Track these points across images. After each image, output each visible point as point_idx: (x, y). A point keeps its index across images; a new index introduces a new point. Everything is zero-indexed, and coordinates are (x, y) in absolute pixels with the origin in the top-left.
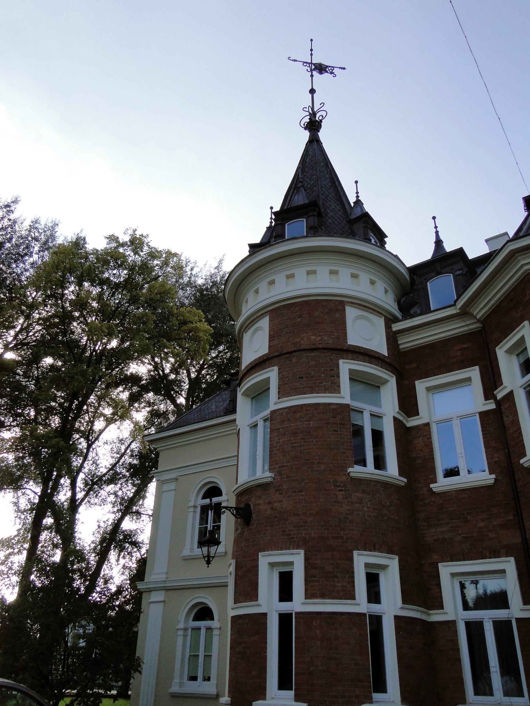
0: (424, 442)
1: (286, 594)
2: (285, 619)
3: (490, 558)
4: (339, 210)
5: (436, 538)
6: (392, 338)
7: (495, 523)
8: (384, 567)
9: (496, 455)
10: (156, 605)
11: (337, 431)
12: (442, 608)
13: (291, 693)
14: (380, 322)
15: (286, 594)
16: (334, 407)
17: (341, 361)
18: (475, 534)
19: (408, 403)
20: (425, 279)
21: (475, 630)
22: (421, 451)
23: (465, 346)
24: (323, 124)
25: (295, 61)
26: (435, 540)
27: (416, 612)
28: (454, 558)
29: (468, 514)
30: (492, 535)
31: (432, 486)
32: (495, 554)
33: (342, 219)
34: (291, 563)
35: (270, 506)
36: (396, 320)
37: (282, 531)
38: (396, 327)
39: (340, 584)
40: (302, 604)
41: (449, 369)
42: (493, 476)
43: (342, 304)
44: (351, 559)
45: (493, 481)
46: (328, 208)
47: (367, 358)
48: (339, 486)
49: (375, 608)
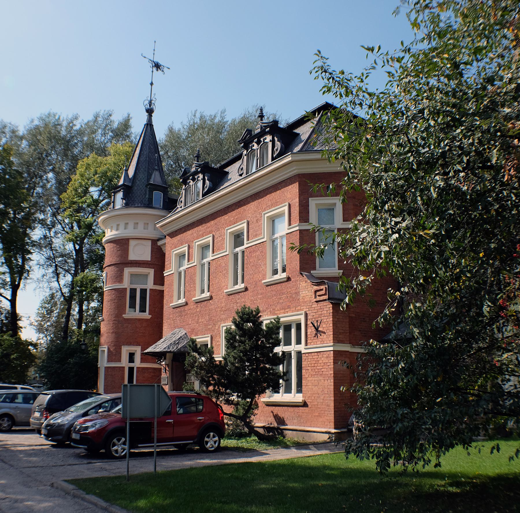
25: (145, 57)
47: (138, 265)
49: (131, 365)
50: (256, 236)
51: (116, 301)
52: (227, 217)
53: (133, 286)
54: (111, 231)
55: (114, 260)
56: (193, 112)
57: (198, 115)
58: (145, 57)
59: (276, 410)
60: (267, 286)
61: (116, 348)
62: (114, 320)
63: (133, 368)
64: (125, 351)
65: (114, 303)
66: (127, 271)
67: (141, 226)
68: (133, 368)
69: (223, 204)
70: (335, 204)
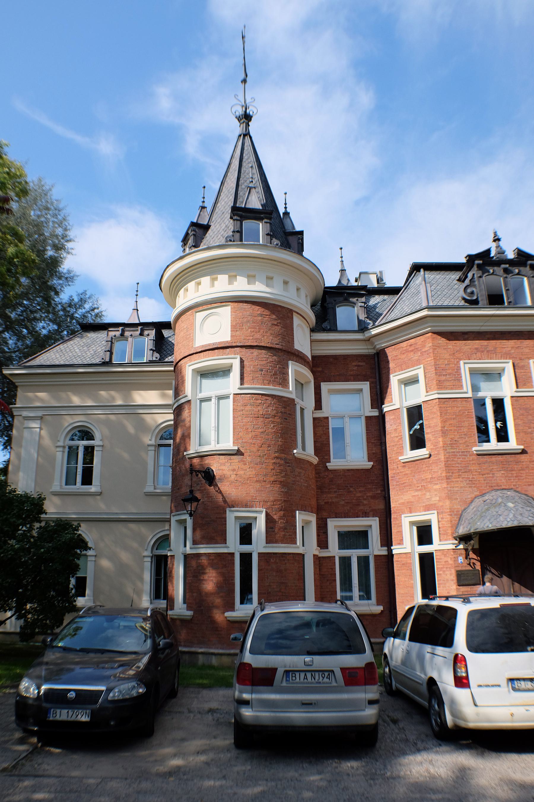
0: (323, 431)
3: (363, 517)
7: (368, 495)
8: (370, 526)
9: (374, 449)
12: (328, 548)
16: (285, 399)
17: (290, 363)
20: (335, 301)
23: (360, 364)
26: (325, 503)
27: (212, 549)
28: (337, 516)
29: (351, 487)
30: (365, 502)
31: (328, 464)
32: (366, 515)
35: (235, 473)
37: (246, 493)
39: (288, 534)
40: (264, 547)
41: (347, 379)
42: (372, 463)
43: (291, 311)
48: (288, 463)
49: (246, 548)
50: (525, 385)
61: (284, 515)
62: (277, 458)
65: (273, 422)
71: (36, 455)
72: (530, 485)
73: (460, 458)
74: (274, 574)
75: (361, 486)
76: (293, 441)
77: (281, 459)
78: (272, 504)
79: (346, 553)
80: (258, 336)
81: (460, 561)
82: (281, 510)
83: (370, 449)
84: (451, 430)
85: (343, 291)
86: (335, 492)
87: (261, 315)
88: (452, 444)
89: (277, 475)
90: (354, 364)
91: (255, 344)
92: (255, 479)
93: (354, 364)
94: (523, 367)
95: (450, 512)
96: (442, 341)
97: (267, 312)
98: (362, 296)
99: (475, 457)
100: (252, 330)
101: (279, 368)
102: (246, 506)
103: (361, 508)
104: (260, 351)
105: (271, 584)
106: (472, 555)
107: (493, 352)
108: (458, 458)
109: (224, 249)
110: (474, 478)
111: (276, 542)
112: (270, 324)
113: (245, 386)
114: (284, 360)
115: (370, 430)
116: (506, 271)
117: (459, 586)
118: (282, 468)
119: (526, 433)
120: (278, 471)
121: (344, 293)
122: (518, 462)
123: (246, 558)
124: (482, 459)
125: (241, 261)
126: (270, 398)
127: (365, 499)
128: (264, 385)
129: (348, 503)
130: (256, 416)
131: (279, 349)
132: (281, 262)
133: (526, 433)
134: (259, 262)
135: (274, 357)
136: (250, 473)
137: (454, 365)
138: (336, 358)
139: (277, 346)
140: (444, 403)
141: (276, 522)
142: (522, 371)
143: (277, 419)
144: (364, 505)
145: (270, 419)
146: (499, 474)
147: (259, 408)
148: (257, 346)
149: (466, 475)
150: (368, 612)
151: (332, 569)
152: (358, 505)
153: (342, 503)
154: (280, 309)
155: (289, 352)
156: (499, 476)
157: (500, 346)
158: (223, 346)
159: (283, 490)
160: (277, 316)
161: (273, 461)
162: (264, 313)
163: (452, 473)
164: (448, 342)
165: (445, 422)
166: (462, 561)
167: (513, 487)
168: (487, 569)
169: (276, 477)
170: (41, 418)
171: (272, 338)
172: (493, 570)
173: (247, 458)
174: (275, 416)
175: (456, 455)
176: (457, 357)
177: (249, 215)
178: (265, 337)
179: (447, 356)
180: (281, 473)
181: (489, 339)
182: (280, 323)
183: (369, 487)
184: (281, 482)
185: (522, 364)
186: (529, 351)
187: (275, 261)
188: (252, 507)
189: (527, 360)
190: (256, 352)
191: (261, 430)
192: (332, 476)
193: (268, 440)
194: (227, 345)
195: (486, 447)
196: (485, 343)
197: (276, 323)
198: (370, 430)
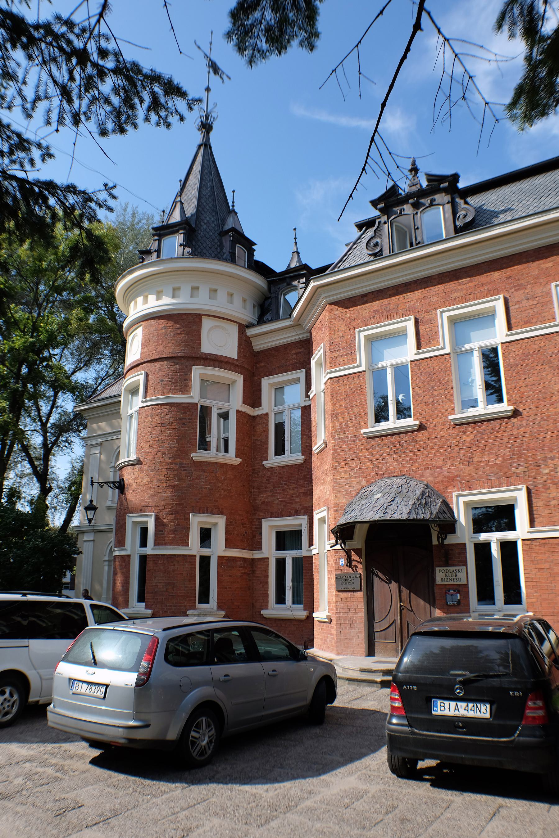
1: (144, 543)
2: (143, 559)
4: (213, 222)
5: (263, 501)
6: (245, 342)
8: (215, 525)
10: (88, 543)
11: (186, 424)
13: (143, 604)
14: (234, 330)
15: (144, 543)
16: (186, 405)
18: (287, 499)
19: (253, 396)
21: (281, 564)
22: (261, 435)
24: (214, 126)
25: (199, 47)
28: (272, 515)
29: (285, 484)
33: (213, 231)
34: (146, 522)
36: (250, 326)
38: (250, 332)
42: (240, 460)
44: (188, 519)
45: (302, 461)
46: (203, 220)
47: (217, 363)
48: (184, 467)
49: (206, 552)
50: (430, 343)
51: (174, 426)
52: (550, 264)
53: (206, 402)
54: (158, 299)
55: (178, 349)
56: (124, 206)
57: (130, 210)
58: (199, 47)
59: (410, 635)
60: (368, 438)
61: (175, 518)
62: (171, 463)
63: (209, 558)
64: (196, 522)
65: (169, 429)
66: (197, 373)
67: (222, 295)
68: (209, 558)
69: (514, 246)
70: (234, 382)
71: (97, 476)
72: (428, 468)
73: (348, 444)
74: (162, 574)
75: (294, 483)
76: (192, 445)
77: (176, 464)
78: (163, 508)
79: (282, 554)
80: (160, 348)
81: (341, 563)
82: (172, 514)
83: (304, 442)
84: (341, 413)
85: (284, 277)
86: (271, 491)
87: (165, 327)
88: (341, 429)
89: (170, 480)
90: (293, 352)
91: (157, 357)
92: (150, 486)
93: (293, 352)
94: (429, 321)
95: (334, 507)
96: (339, 311)
97: (170, 323)
98: (301, 276)
99: (364, 441)
100: (156, 344)
101: (181, 375)
102: (141, 511)
103: (293, 506)
104: (162, 363)
105: (158, 584)
106: (354, 556)
107: (395, 310)
108: (346, 445)
109: (132, 273)
110: (362, 466)
111: (166, 544)
112: (172, 334)
113: (148, 399)
114: (187, 366)
115: (305, 421)
116: (416, 206)
117: (339, 591)
118: (176, 472)
119: (426, 404)
120: (171, 476)
121: (285, 278)
122: (414, 442)
123: (205, 561)
124: (374, 442)
125: (149, 280)
126: (168, 407)
127: (297, 497)
128: (164, 395)
129: (281, 501)
130: (155, 425)
131: (181, 357)
132: (184, 271)
133: (426, 404)
134: (163, 277)
135: (175, 366)
136: (146, 480)
137: (349, 337)
138: (277, 349)
139: (179, 355)
140: (336, 382)
141: (166, 525)
142: (427, 326)
143: (174, 426)
144: (296, 503)
145: (167, 427)
146: (389, 459)
147: (158, 418)
148: (159, 359)
149: (352, 463)
150: (292, 617)
151: (265, 571)
152: (291, 503)
153: (277, 502)
154: (185, 317)
155: (193, 358)
156: (391, 462)
157: (404, 301)
158: (136, 364)
159: (175, 494)
160: (181, 325)
161: (167, 467)
162: (168, 325)
163: (339, 462)
164: (345, 310)
165: (335, 404)
166: (343, 563)
167: (406, 473)
168: (374, 573)
169: (168, 482)
170: (101, 444)
171: (173, 347)
172: (380, 574)
173: (145, 467)
174: (172, 423)
175: (344, 442)
176: (351, 327)
177: (166, 231)
178: (167, 348)
179: (343, 328)
180: (174, 478)
181: (390, 296)
182: (184, 331)
183: (302, 483)
184: (174, 486)
185: (428, 317)
186: (439, 299)
187: (177, 271)
188: (145, 512)
189: (434, 312)
190: (158, 364)
191: (157, 439)
192: (269, 474)
193: (163, 447)
194: (139, 362)
195: (383, 426)
196: (385, 301)
197: (179, 332)
198: (305, 421)
